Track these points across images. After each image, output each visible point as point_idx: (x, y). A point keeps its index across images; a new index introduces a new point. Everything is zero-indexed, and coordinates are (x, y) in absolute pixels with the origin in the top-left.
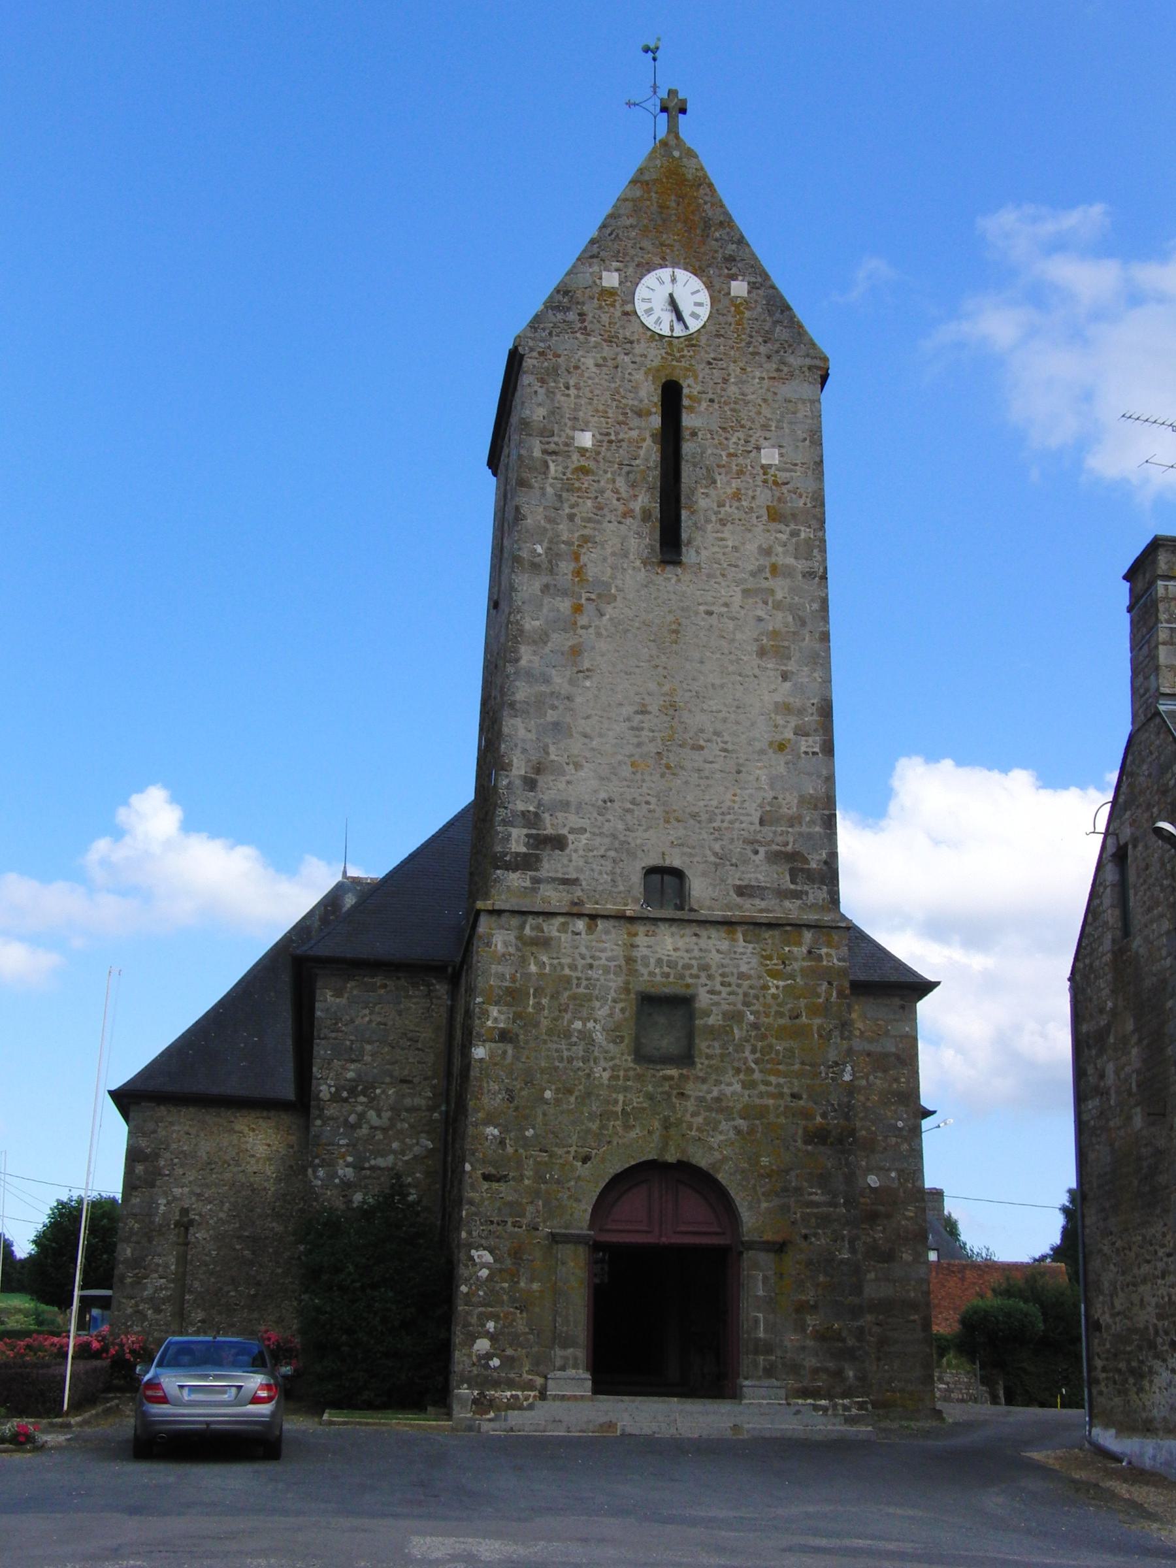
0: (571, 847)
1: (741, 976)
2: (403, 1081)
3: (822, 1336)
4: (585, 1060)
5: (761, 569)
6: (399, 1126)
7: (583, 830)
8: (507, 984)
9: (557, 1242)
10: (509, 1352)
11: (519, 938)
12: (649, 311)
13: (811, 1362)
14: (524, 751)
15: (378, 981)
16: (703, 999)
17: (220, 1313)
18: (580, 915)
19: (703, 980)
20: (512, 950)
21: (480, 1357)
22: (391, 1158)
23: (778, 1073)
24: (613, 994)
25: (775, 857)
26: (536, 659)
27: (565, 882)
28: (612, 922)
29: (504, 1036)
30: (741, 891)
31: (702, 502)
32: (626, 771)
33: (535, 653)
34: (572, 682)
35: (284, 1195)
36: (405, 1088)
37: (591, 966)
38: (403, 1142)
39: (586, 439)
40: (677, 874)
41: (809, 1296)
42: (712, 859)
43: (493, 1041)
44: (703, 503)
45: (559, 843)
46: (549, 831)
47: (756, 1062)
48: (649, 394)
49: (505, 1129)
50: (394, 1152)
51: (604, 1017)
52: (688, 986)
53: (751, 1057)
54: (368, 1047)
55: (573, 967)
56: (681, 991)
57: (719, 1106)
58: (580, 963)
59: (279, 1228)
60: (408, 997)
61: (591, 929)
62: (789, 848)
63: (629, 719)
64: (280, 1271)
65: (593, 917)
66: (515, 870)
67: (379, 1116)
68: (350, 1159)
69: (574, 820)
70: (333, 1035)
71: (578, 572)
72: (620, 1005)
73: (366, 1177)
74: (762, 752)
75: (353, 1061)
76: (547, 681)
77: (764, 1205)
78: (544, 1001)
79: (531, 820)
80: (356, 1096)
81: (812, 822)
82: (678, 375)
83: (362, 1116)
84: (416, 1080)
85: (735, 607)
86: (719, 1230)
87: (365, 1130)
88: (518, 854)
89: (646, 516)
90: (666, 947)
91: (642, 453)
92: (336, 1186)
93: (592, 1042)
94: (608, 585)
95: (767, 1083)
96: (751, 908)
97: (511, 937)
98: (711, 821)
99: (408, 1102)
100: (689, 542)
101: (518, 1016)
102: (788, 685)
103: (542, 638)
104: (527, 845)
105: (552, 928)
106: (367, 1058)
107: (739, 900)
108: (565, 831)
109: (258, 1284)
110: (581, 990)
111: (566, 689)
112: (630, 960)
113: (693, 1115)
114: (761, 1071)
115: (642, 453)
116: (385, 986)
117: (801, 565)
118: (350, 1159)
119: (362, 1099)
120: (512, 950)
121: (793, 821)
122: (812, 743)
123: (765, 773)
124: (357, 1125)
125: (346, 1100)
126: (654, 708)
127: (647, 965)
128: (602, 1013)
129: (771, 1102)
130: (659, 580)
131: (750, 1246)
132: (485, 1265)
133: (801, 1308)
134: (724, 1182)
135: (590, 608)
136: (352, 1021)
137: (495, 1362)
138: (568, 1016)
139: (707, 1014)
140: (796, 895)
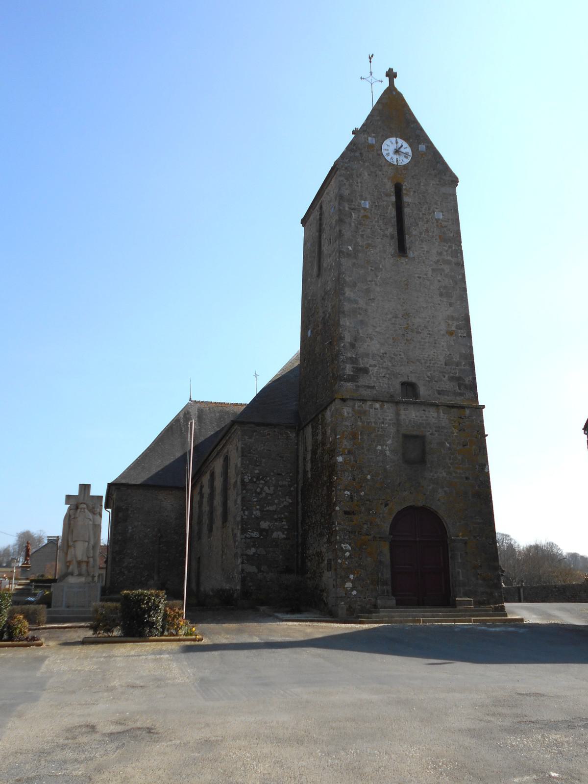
14: (349, 332)
22: (275, 506)
30: (440, 392)
32: (391, 341)
45: (365, 371)
48: (390, 187)
54: (264, 460)
61: (382, 407)
66: (349, 382)
68: (258, 507)
69: (372, 362)
79: (354, 361)
88: (349, 375)
90: (412, 415)
96: (445, 399)
104: (353, 371)
106: (263, 465)
118: (258, 507)
119: (262, 482)
125: (255, 482)
140: (461, 395)
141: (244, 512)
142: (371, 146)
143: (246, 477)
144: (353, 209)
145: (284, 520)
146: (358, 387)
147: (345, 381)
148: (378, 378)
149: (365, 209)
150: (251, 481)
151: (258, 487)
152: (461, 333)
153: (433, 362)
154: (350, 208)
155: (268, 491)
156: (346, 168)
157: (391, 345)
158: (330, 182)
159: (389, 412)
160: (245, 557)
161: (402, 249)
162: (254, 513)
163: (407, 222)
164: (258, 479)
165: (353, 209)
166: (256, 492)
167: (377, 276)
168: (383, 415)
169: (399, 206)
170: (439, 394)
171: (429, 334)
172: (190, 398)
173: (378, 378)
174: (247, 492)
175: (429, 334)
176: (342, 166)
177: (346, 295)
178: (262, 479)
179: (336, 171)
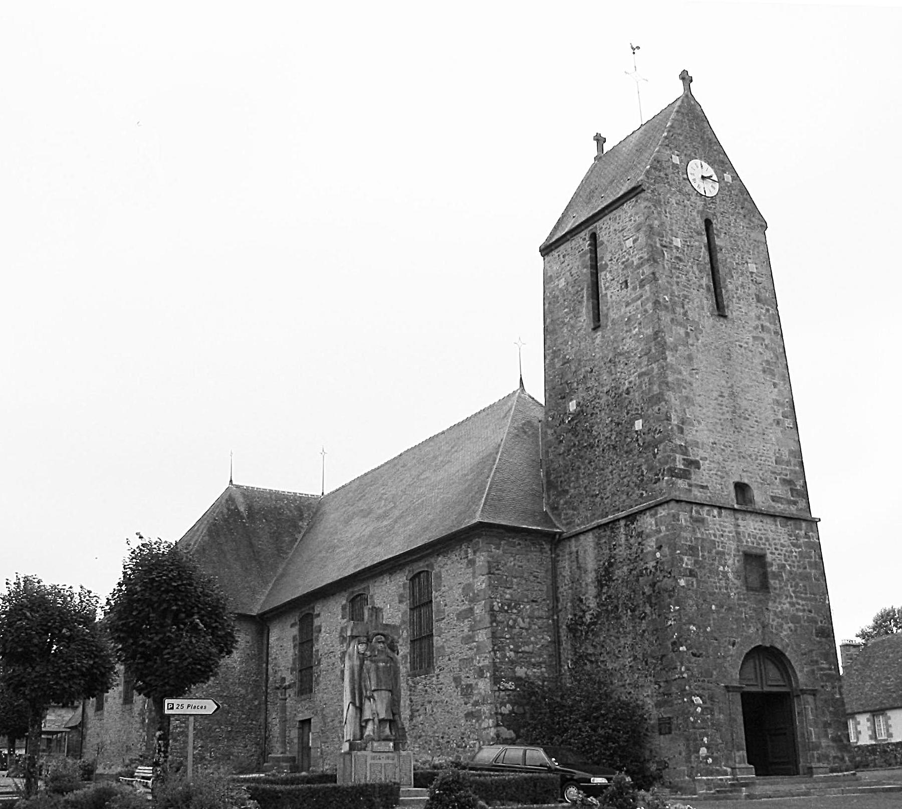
0: (702, 467)
1: (783, 546)
2: (533, 601)
3: (834, 740)
4: (727, 589)
5: (756, 328)
6: (533, 627)
7: (705, 459)
8: (689, 543)
9: (729, 691)
10: (715, 754)
11: (691, 517)
12: (694, 180)
13: (833, 753)
14: (676, 411)
15: (516, 541)
16: (769, 557)
17: (211, 742)
18: (715, 506)
19: (768, 546)
20: (688, 524)
21: (704, 758)
22: (531, 646)
23: (802, 599)
24: (733, 552)
25: (785, 482)
26: (674, 359)
27: (702, 487)
28: (728, 512)
29: (692, 573)
30: (774, 499)
31: (730, 286)
32: (719, 428)
33: (673, 356)
34: (691, 374)
35: (246, 671)
36: (534, 604)
37: (722, 536)
38: (536, 637)
39: (678, 242)
40: (746, 485)
41: (828, 718)
42: (759, 480)
43: (686, 576)
44: (730, 286)
45: (696, 464)
46: (692, 458)
47: (794, 592)
48: (700, 224)
49: (698, 628)
50: (532, 643)
51: (732, 564)
52: (762, 549)
53: (791, 590)
54: (515, 580)
55: (715, 536)
56: (758, 551)
57: (779, 615)
58: (718, 533)
59: (243, 692)
60: (531, 551)
61: (720, 515)
62: (788, 477)
63: (716, 399)
64: (244, 716)
65: (720, 508)
66: (681, 478)
67: (523, 621)
68: (512, 647)
69: (702, 453)
70: (497, 572)
71: (685, 314)
72: (737, 558)
73: (521, 657)
74: (771, 425)
75: (508, 588)
76: (680, 373)
77: (805, 669)
78: (706, 554)
79: (684, 450)
80: (512, 609)
81: (795, 465)
82: (711, 217)
83: (515, 621)
84: (539, 600)
85: (750, 344)
86: (783, 684)
87: (517, 630)
88: (680, 469)
89: (708, 287)
90: (751, 526)
91: (702, 254)
92: (507, 663)
93: (728, 579)
94: (698, 323)
95: (799, 604)
96: (780, 507)
97: (688, 516)
98: (757, 459)
99: (536, 613)
100: (728, 307)
101: (696, 562)
102: (776, 390)
103: (675, 349)
104: (683, 464)
105: (704, 512)
106: (515, 587)
107: (773, 504)
108: (698, 458)
109: (232, 724)
110: (720, 549)
111: (689, 379)
112: (738, 533)
113: (773, 620)
114: (796, 597)
115: (702, 254)
116: (519, 544)
117: (772, 327)
118: (512, 647)
119: (515, 611)
120: (688, 524)
121: (788, 463)
122: (788, 423)
123: (775, 434)
124: (512, 627)
125: (506, 611)
126: (726, 394)
127: (744, 537)
128: (730, 562)
129: (801, 614)
130: (718, 324)
131: (803, 692)
132: (699, 705)
133: (826, 725)
134: (789, 657)
135: (692, 334)
136: (506, 564)
137: (710, 761)
138: (716, 563)
139: (772, 565)
140: (795, 503)
141: (495, 654)
142: (675, 166)
143: (495, 603)
144: (665, 246)
145: (543, 666)
146: (690, 485)
147: (677, 477)
148: (713, 479)
149: (677, 248)
150: (501, 609)
151: (510, 619)
152: (788, 423)
153: (763, 458)
154: (661, 245)
155: (522, 625)
156: (652, 191)
157: (719, 432)
158: (623, 204)
159: (728, 520)
160: (500, 717)
161: (720, 310)
162: (508, 655)
163: (722, 271)
164: (509, 606)
165: (665, 246)
166: (508, 625)
167: (698, 340)
168: (720, 526)
169: (711, 248)
170: (773, 501)
171: (756, 421)
172: (231, 481)
173: (713, 479)
174: (497, 626)
175: (756, 421)
176: (648, 188)
177: (668, 360)
178: (515, 607)
179: (640, 193)
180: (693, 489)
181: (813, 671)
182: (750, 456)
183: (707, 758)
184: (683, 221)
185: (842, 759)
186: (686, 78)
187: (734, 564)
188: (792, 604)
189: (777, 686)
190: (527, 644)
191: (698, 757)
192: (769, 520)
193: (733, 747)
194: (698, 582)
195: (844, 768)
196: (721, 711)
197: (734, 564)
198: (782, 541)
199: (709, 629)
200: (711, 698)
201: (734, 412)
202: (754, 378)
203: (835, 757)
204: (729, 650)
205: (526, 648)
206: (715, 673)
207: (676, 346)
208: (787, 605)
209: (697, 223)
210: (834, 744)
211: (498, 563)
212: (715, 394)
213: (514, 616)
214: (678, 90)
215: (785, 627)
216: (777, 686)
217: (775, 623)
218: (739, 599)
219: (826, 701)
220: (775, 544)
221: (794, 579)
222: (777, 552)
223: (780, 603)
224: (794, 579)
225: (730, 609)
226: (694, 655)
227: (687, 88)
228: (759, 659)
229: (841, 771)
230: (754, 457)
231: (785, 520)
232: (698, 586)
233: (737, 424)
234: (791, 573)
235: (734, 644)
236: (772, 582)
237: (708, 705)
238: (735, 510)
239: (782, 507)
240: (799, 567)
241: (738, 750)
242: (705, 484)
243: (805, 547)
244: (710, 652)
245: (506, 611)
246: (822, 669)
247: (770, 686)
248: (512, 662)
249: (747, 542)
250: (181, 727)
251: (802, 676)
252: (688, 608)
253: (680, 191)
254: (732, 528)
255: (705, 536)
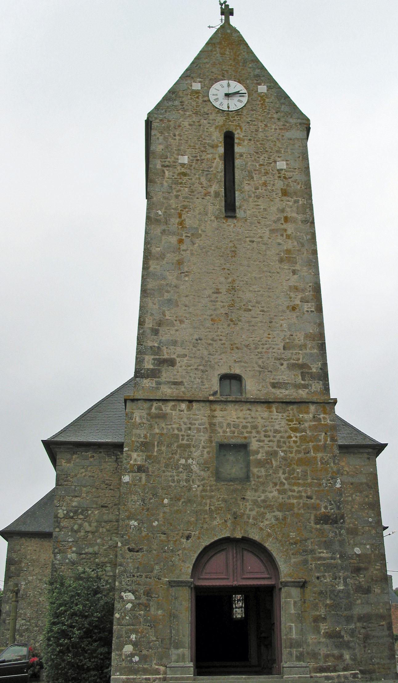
1: (276, 431)
2: (102, 506)
6: (101, 530)
9: (172, 586)
10: (144, 652)
11: (149, 414)
13: (324, 651)
16: (254, 445)
18: (183, 401)
19: (254, 434)
20: (144, 421)
21: (127, 656)
27: (175, 383)
29: (140, 469)
30: (274, 386)
41: (322, 612)
49: (141, 522)
50: (97, 544)
52: (245, 438)
53: (282, 476)
54: (84, 489)
55: (179, 429)
56: (240, 441)
58: (183, 427)
61: (189, 409)
63: (209, 297)
65: (191, 401)
67: (90, 525)
70: (66, 483)
72: (206, 450)
76: (164, 278)
77: (293, 560)
78: (164, 448)
83: (80, 526)
86: (268, 576)
87: (82, 534)
88: (148, 369)
92: (67, 564)
93: (191, 471)
101: (148, 457)
102: (296, 276)
104: (153, 364)
105: (167, 408)
106: (84, 495)
107: (273, 390)
113: (251, 510)
116: (93, 457)
117: (300, 217)
118: (74, 549)
119: (81, 517)
125: (72, 518)
126: (223, 290)
128: (196, 454)
131: (286, 584)
136: (76, 476)
137: (136, 659)
138: (177, 457)
140: (305, 387)
143: (60, 511)
155: (88, 528)
164: (75, 512)
178: (82, 513)
180: (162, 386)
181: (306, 562)
182: (247, 346)
183: (132, 655)
184: (196, 138)
185: (340, 657)
186: (227, 12)
187: (202, 455)
188: (282, 492)
189: (253, 578)
190: (91, 545)
191: (121, 655)
192: (260, 408)
193: (171, 644)
194: (148, 476)
195: (341, 667)
196: (159, 606)
197: (202, 455)
198: (277, 427)
199: (155, 524)
200: (148, 594)
201: (232, 306)
202: (265, 269)
203: (327, 656)
204: (181, 543)
205: (90, 550)
206: (157, 567)
207: (164, 255)
208: (276, 493)
209: (214, 137)
210: (328, 641)
211: (67, 475)
212: (208, 292)
213: (79, 522)
214: (217, 21)
215: (268, 516)
216: (253, 578)
217: (254, 513)
218: (203, 490)
219: (321, 593)
220: (266, 431)
221: (289, 465)
222: (266, 439)
223: (264, 491)
224: (289, 465)
225: (189, 501)
226: (130, 550)
227: (227, 20)
228: (236, 550)
229: (335, 671)
230: (253, 346)
231: (284, 406)
232: (148, 481)
233: (234, 317)
234: (284, 459)
235: (188, 537)
236: (255, 470)
237: (144, 600)
238: (211, 402)
239: (287, 392)
240: (298, 452)
241: (177, 648)
242: (180, 380)
243: (310, 431)
244: (155, 546)
245: (72, 518)
246: (320, 558)
247: (244, 579)
248: (73, 563)
249: (224, 432)
250: (25, 625)
251: (286, 569)
252: (129, 505)
253: (196, 113)
254: (205, 420)
255: (165, 431)
